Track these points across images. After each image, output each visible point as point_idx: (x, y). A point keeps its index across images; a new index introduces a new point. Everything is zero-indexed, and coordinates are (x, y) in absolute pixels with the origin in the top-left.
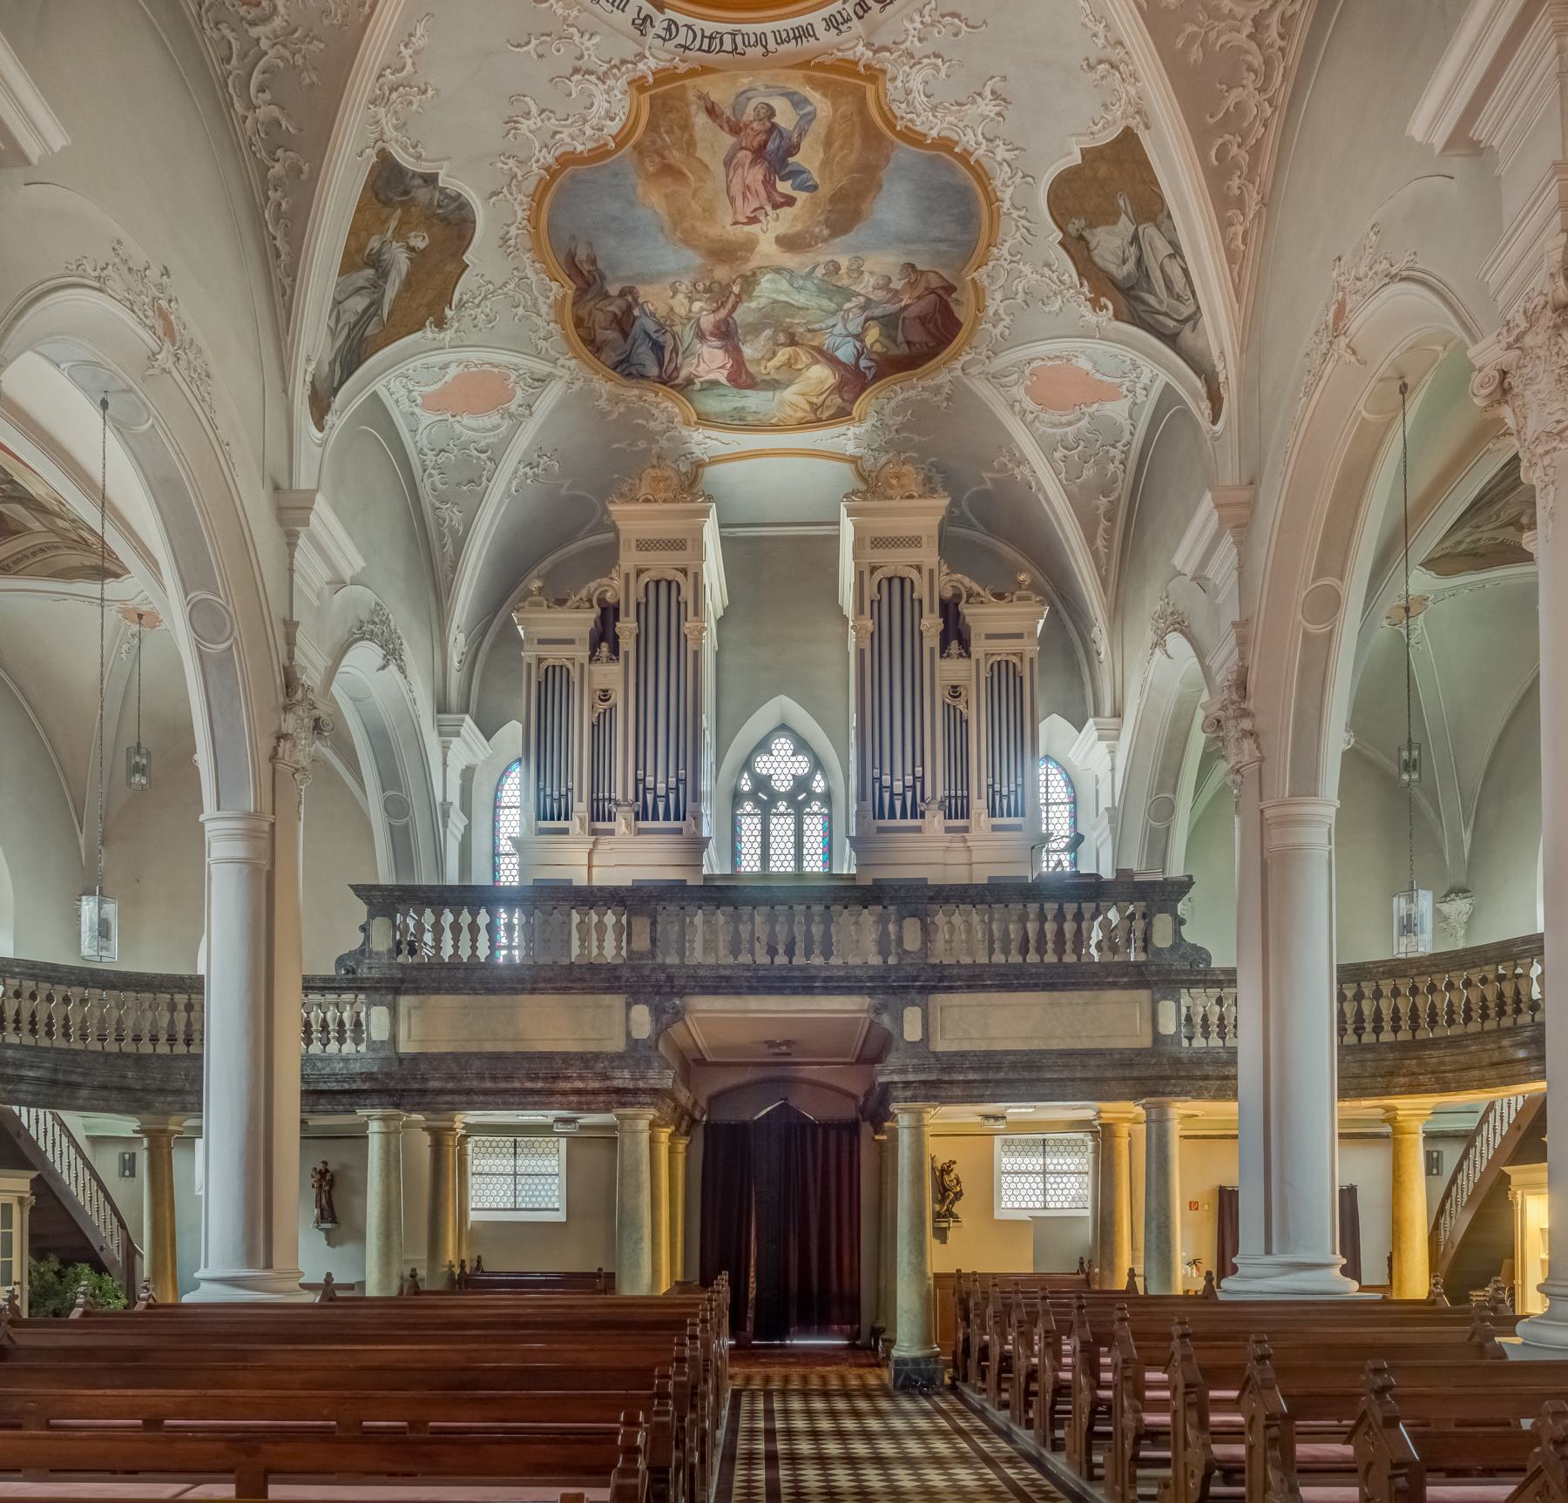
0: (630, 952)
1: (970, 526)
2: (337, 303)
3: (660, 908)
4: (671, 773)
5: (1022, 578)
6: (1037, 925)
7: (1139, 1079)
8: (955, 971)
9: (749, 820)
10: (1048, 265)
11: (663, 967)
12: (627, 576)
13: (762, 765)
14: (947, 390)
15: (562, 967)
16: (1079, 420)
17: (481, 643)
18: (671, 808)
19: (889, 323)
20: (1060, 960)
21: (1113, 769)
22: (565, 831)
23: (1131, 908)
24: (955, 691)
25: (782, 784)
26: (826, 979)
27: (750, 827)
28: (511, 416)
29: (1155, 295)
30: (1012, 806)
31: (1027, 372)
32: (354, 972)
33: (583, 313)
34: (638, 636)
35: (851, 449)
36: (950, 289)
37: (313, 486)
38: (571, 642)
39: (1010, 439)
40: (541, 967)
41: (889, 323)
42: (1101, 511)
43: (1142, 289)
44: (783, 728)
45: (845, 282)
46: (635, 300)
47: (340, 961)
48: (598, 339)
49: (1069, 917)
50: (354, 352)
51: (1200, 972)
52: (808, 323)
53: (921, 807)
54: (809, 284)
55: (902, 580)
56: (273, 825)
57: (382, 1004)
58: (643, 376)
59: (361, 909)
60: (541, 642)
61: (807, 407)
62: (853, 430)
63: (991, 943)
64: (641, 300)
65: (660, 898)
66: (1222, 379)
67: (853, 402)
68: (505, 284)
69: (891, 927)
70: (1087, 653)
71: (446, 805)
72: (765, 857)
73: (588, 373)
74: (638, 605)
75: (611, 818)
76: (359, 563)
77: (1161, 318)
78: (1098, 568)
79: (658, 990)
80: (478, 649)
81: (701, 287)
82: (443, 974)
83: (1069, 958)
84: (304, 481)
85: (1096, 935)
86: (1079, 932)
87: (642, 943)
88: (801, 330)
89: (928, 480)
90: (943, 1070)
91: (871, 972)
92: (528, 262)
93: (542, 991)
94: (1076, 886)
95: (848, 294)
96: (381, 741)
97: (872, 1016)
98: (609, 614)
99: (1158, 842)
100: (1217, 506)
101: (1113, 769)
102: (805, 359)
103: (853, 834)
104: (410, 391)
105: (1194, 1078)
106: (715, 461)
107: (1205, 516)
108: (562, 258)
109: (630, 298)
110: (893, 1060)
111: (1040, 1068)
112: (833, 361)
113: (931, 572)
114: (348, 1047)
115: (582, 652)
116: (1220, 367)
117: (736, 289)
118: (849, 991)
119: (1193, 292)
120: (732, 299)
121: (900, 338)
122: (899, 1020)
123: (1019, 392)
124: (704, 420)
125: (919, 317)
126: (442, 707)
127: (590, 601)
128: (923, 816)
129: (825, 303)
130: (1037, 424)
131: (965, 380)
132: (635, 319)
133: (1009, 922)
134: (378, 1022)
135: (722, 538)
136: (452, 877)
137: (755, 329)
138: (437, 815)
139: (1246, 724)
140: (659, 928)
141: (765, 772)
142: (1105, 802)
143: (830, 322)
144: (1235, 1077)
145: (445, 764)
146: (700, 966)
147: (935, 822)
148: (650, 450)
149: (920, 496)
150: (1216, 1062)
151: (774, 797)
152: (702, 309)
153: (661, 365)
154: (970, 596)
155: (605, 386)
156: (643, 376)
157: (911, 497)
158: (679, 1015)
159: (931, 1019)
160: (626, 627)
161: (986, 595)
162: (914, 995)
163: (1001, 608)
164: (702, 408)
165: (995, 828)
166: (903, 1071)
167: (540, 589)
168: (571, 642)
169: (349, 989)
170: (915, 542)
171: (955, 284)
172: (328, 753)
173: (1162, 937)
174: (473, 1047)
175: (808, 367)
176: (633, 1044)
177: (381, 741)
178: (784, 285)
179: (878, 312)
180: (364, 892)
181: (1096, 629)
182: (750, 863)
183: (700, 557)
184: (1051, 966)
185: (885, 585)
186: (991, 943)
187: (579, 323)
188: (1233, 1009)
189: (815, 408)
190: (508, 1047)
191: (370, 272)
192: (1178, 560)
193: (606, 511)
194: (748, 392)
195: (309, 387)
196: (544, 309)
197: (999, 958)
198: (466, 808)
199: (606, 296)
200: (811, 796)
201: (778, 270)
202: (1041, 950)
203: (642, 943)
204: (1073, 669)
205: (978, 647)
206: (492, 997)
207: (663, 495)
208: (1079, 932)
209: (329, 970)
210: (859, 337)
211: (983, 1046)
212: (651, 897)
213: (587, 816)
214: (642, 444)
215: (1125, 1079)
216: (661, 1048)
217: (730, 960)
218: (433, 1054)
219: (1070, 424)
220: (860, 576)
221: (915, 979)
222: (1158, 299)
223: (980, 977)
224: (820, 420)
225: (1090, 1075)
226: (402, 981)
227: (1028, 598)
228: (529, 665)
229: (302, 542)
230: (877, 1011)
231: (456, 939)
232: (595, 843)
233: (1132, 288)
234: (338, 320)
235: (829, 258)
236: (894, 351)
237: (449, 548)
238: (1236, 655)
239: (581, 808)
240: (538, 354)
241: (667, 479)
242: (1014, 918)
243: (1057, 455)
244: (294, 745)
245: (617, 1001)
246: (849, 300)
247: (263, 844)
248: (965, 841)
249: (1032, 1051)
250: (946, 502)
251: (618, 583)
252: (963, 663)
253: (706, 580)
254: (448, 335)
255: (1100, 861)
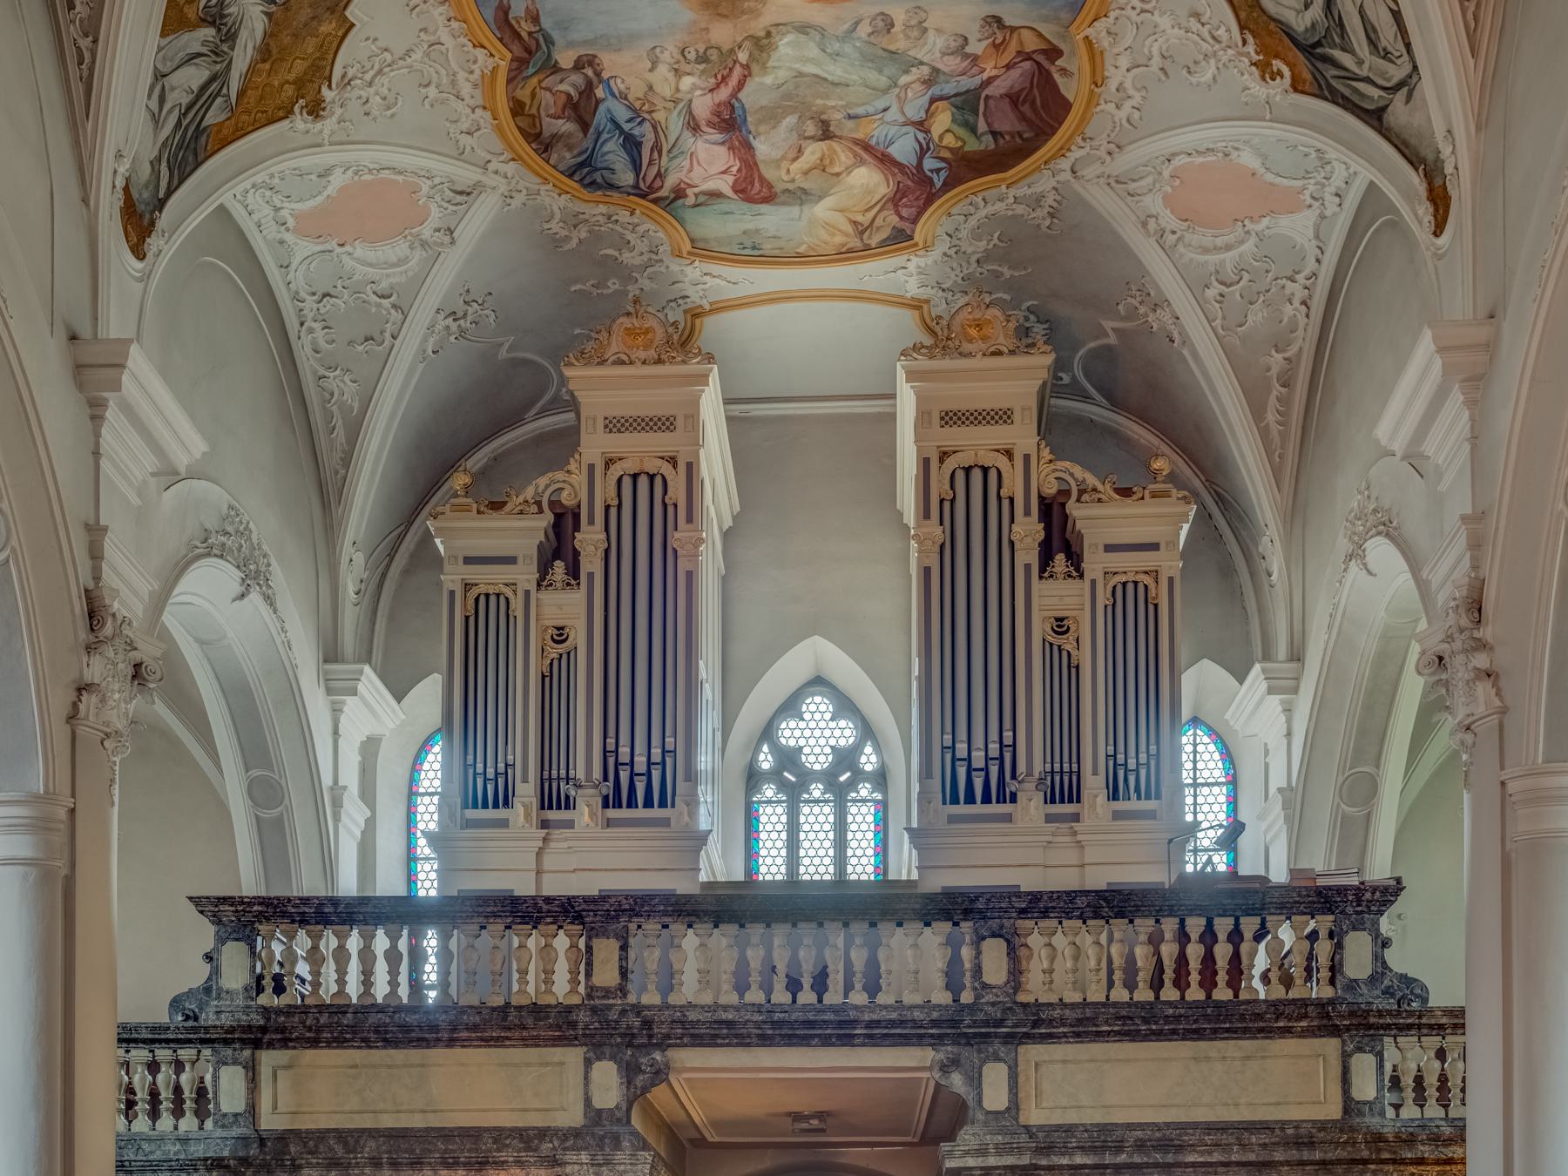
0: (591, 989)
1: (1086, 398)
2: (159, 76)
3: (632, 926)
4: (656, 740)
5: (1157, 465)
6: (1175, 948)
7: (1323, 1163)
8: (1057, 1013)
9: (769, 810)
10: (1197, 15)
11: (638, 1009)
12: (591, 467)
13: (789, 734)
14: (1050, 201)
15: (494, 1009)
16: (1242, 242)
17: (388, 566)
18: (641, 790)
19: (967, 104)
20: (1209, 996)
21: (1289, 734)
22: (504, 824)
23: (1312, 925)
24: (1061, 626)
25: (817, 759)
26: (871, 1024)
27: (772, 819)
28: (424, 244)
29: (1352, 52)
30: (1138, 782)
31: (1166, 174)
32: (196, 1019)
33: (523, 94)
34: (607, 551)
35: (913, 289)
36: (1053, 53)
37: (130, 333)
38: (512, 560)
39: (1144, 272)
40: (463, 1010)
41: (967, 104)
42: (1274, 372)
43: (1334, 46)
44: (818, 683)
45: (900, 44)
46: (598, 74)
47: (176, 1003)
48: (546, 133)
49: (1222, 936)
50: (189, 148)
51: (1411, 1014)
52: (848, 105)
53: (1012, 786)
54: (848, 49)
55: (985, 470)
56: (73, 811)
57: (235, 1063)
58: (611, 186)
59: (205, 934)
60: (468, 560)
61: (849, 229)
62: (915, 262)
63: (1111, 972)
64: (605, 75)
65: (633, 913)
66: (1449, 169)
67: (915, 221)
68: (408, 53)
69: (966, 953)
70: (1253, 574)
71: (337, 790)
72: (793, 860)
73: (532, 181)
74: (607, 508)
75: (568, 804)
76: (199, 446)
77: (1361, 86)
78: (1269, 453)
79: (629, 1039)
80: (384, 575)
81: (692, 56)
82: (324, 1019)
83: (1222, 993)
84: (115, 325)
85: (1261, 962)
86: (1236, 958)
87: (607, 975)
88: (838, 116)
89: (1023, 332)
90: (1039, 1151)
91: (935, 1015)
92: (441, 20)
93: (465, 1043)
94: (1232, 894)
95: (910, 64)
96: (239, 696)
97: (937, 1075)
98: (565, 521)
99: (1353, 831)
100: (1441, 350)
101: (1289, 734)
102: (844, 157)
103: (915, 825)
104: (277, 209)
105: (1403, 1162)
106: (718, 308)
107: (1422, 363)
108: (490, 14)
109: (589, 72)
110: (968, 1137)
111: (1180, 1148)
112: (885, 160)
113: (1027, 458)
114: (188, 1123)
115: (525, 574)
116: (1446, 151)
117: (743, 57)
118: (905, 1041)
119: (1408, 46)
120: (738, 71)
121: (982, 126)
122: (976, 1081)
123: (1153, 203)
124: (701, 250)
125: (1008, 95)
126: (331, 654)
127: (539, 504)
128: (1014, 799)
129: (873, 77)
130: (1181, 248)
131: (1077, 186)
132: (598, 102)
133: (1129, 942)
134: (230, 1089)
135: (729, 419)
136: (347, 884)
137: (772, 116)
138: (325, 803)
139: (1481, 661)
140: (632, 954)
141: (792, 743)
142: (1278, 779)
143: (881, 104)
144: (1463, 1161)
145: (336, 732)
146: (691, 1006)
147: (1031, 806)
148: (626, 293)
149: (1012, 353)
150: (1436, 1139)
151: (806, 777)
152: (694, 87)
153: (636, 166)
154: (1081, 492)
155: (558, 201)
156: (611, 186)
157: (998, 353)
158: (660, 1074)
159: (1021, 1079)
160: (590, 540)
161: (1107, 490)
162: (997, 1046)
163: (1129, 508)
164: (698, 232)
165: (1117, 816)
166: (982, 1152)
167: (466, 487)
168: (512, 560)
169: (190, 1041)
170: (1003, 416)
171: (1062, 46)
172: (161, 709)
173: (1358, 963)
174: (366, 1122)
175: (849, 170)
176: (596, 1116)
177: (239, 696)
178: (813, 51)
179: (949, 89)
180: (212, 907)
181: (1266, 540)
182: (772, 867)
183: (696, 442)
184: (1196, 1004)
185: (960, 476)
186: (1111, 972)
187: (517, 109)
188: (1460, 1065)
189: (861, 230)
190: (417, 1122)
191: (208, 32)
192: (1382, 432)
193: (563, 381)
194: (764, 208)
195: (120, 194)
196: (466, 89)
197: (1120, 994)
198: (368, 794)
199: (556, 69)
200: (858, 775)
201: (803, 29)
202: (1181, 982)
203: (607, 975)
204: (1233, 594)
205: (1095, 561)
206: (392, 1052)
207: (642, 355)
208: (1236, 958)
209: (161, 1015)
210: (921, 125)
211: (1098, 1117)
212: (620, 911)
213: (535, 802)
214: (613, 285)
215: (1302, 1163)
216: (636, 1122)
217: (734, 999)
218: (308, 1132)
219: (1228, 248)
220: (925, 464)
221: (1000, 1023)
222: (1357, 58)
223: (1092, 1021)
224: (868, 248)
225: (1252, 1157)
226: (264, 1029)
227: (1165, 494)
228: (452, 593)
229: (112, 414)
230: (945, 1068)
231: (394, 973)
232: (545, 840)
233: (1319, 44)
234: (162, 100)
235: (876, 9)
236: (972, 145)
237: (340, 434)
238: (1466, 562)
239: (526, 792)
240: (460, 155)
241: (647, 332)
242: (1143, 938)
243: (1211, 293)
244: (103, 700)
245: (573, 1056)
246: (907, 72)
247: (60, 839)
248: (1075, 834)
249: (1168, 1125)
250: (1049, 359)
251: (579, 479)
252: (1073, 586)
253: (704, 472)
254: (327, 126)
255: (1271, 857)
